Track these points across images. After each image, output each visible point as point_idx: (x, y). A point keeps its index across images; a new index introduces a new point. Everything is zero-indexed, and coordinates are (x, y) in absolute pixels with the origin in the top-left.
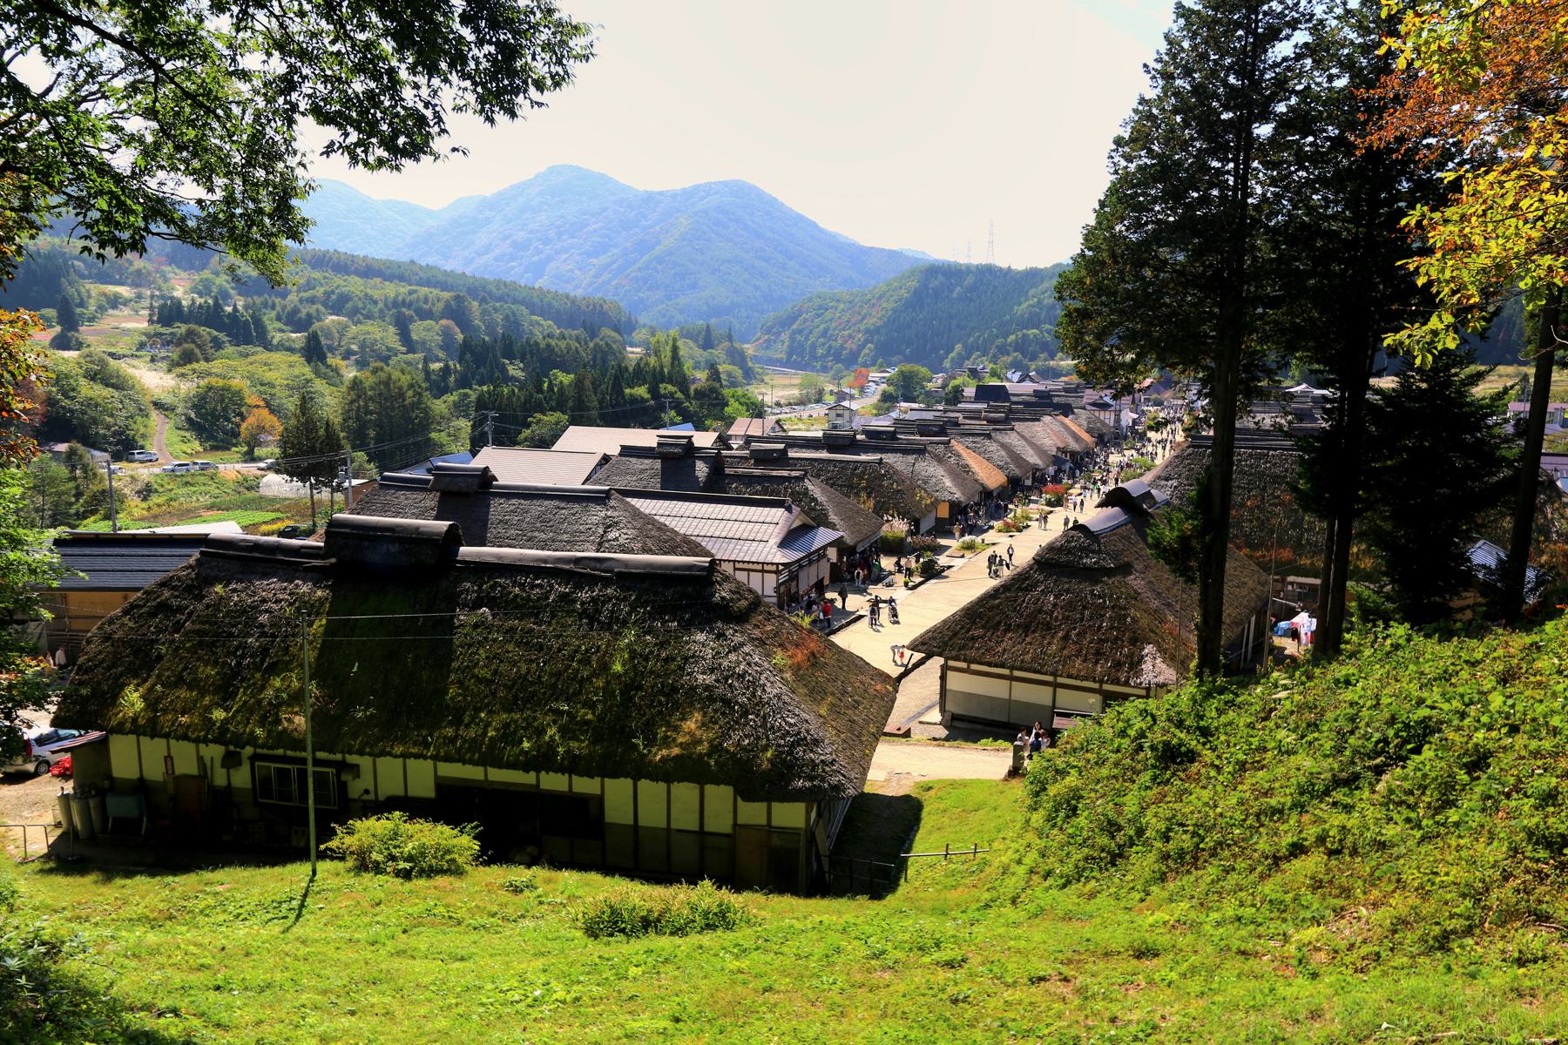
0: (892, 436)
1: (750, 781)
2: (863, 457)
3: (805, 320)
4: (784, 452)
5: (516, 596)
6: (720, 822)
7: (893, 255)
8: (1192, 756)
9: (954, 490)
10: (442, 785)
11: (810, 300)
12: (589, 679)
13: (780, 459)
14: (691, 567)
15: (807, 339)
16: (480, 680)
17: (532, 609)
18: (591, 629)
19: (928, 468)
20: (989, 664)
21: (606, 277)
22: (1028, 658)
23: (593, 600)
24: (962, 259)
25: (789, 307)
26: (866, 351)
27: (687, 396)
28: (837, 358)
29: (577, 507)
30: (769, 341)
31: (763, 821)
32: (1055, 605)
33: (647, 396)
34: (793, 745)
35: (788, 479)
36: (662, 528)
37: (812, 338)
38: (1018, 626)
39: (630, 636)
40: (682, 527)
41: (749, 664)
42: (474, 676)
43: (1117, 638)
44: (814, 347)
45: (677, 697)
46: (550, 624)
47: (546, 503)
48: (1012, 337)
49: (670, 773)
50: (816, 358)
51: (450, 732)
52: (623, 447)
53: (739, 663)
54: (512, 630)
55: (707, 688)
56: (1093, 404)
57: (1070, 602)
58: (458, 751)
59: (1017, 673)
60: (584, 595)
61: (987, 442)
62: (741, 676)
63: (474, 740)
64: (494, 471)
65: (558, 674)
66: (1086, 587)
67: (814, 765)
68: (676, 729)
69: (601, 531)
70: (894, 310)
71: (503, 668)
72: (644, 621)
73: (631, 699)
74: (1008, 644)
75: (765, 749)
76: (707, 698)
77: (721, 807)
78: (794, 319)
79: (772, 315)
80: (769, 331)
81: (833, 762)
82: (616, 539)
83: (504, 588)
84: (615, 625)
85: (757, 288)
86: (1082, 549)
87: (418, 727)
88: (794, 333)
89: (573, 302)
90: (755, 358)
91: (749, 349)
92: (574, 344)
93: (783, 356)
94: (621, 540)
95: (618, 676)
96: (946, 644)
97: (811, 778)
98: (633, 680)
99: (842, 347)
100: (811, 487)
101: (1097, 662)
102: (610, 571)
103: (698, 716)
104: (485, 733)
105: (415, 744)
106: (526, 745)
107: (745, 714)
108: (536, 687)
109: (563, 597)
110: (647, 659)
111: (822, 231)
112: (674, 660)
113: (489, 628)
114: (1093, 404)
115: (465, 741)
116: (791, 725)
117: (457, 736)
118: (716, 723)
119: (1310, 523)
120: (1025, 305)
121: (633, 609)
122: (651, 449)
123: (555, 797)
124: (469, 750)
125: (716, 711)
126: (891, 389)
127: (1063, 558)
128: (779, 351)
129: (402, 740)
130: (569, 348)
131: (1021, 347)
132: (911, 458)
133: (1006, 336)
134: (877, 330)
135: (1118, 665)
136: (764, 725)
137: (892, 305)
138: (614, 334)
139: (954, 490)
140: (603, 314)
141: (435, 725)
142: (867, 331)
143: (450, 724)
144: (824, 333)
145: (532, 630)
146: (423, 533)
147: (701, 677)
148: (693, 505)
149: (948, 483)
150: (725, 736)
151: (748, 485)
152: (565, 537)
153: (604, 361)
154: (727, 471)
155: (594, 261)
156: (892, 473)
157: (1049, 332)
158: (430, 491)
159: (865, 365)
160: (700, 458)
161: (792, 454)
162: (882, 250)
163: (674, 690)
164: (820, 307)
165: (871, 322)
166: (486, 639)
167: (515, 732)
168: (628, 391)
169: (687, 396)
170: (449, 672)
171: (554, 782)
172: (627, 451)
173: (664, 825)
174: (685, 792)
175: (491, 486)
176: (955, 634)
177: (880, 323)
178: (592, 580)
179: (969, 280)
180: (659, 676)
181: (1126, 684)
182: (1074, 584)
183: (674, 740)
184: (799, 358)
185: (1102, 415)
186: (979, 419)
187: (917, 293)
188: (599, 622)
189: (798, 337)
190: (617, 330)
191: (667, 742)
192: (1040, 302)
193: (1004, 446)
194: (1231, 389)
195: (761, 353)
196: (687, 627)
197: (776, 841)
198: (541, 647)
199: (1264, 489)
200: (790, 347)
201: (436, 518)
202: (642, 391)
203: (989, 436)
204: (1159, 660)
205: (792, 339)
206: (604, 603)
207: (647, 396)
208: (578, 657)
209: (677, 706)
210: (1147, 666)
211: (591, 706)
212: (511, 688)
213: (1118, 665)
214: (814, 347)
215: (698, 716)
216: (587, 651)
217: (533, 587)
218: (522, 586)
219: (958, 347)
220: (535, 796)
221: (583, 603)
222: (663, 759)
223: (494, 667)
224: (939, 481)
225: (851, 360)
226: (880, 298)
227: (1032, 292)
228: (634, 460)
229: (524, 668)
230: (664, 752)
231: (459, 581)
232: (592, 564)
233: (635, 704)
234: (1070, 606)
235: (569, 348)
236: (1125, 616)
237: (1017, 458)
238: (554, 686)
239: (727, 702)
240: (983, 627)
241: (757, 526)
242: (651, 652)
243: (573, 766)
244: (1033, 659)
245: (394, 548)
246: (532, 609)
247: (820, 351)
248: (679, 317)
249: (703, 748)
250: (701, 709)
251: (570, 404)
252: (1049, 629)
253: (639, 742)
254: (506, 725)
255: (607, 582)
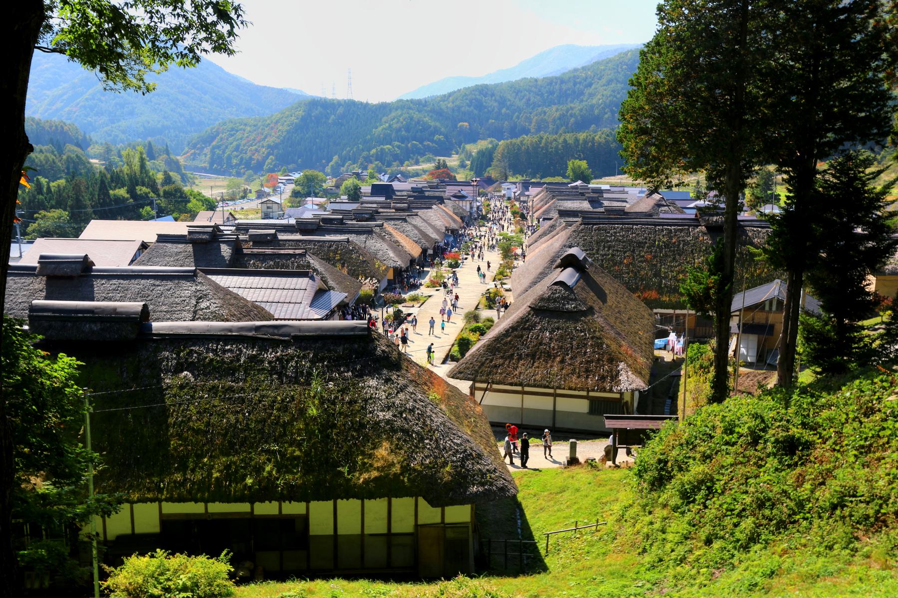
0: (341, 221)
1: (440, 494)
2: (328, 238)
3: (222, 139)
4: (275, 236)
5: (212, 360)
6: (403, 523)
7: (281, 92)
8: (808, 445)
9: (396, 259)
10: (166, 521)
11: (225, 124)
12: (290, 423)
13: (272, 241)
14: (354, 328)
15: (224, 152)
16: (197, 432)
17: (229, 370)
18: (282, 383)
19: (374, 244)
20: (511, 384)
21: (59, 105)
22: (538, 377)
23: (278, 359)
24: (329, 96)
25: (209, 129)
26: (269, 161)
27: (158, 195)
28: (248, 166)
29: (170, 284)
30: (194, 154)
31: (438, 520)
32: (551, 339)
33: (127, 196)
34: (463, 460)
35: (294, 255)
36: (236, 297)
37: (228, 152)
38: (527, 355)
39: (316, 386)
40: (250, 296)
41: (415, 401)
42: (190, 428)
43: (599, 360)
44: (229, 158)
45: (366, 433)
46: (245, 381)
47: (143, 281)
48: (374, 151)
49: (365, 493)
50: (232, 167)
51: (178, 477)
52: (159, 236)
53: (407, 401)
54: (214, 389)
55: (388, 422)
56: (455, 196)
57: (562, 336)
58: (189, 492)
59: (527, 389)
60: (270, 355)
61: (404, 224)
62: (412, 411)
63: (202, 482)
64: (92, 258)
65: (264, 421)
66: (571, 325)
67: (483, 475)
68: (370, 456)
69: (194, 302)
70: (288, 132)
71: (214, 420)
72: (324, 373)
73: (328, 436)
74: (524, 370)
75: (445, 464)
76: (391, 430)
77: (406, 514)
78: (214, 138)
79: (195, 135)
80: (194, 146)
81: (495, 471)
82: (208, 308)
83: (199, 354)
84: (303, 379)
85: (181, 115)
86: (564, 298)
87: (150, 476)
88: (214, 148)
89: (38, 124)
90: (186, 167)
91: (181, 159)
92: (51, 157)
93: (207, 165)
94: (212, 309)
95: (314, 419)
96: (477, 371)
97: (483, 484)
98: (328, 421)
99: (251, 159)
100: (312, 261)
101: (587, 377)
102: (288, 335)
103: (386, 444)
104: (210, 475)
105: (149, 490)
106: (249, 481)
107: (422, 439)
108: (246, 433)
109: (252, 358)
110: (334, 403)
111: (228, 74)
112: (356, 402)
113: (194, 388)
114: (455, 196)
115: (193, 483)
116: (458, 445)
117: (185, 480)
118: (401, 449)
119: (665, 273)
120: (380, 128)
121: (313, 362)
122: (184, 236)
123: (267, 520)
124: (199, 490)
125: (399, 439)
126: (299, 188)
127: (552, 306)
128: (203, 161)
129: (138, 488)
130: (47, 160)
131: (380, 157)
132: (363, 238)
133: (369, 151)
134: (276, 146)
135: (603, 378)
136: (437, 447)
137: (285, 128)
138: (76, 149)
139: (396, 259)
140: (63, 133)
141: (165, 470)
142: (269, 146)
143: (177, 470)
144: (237, 148)
145: (231, 388)
146: (121, 313)
147: (381, 414)
148: (295, 279)
149: (391, 254)
150: (410, 458)
151: (263, 261)
152: (164, 308)
153: (75, 168)
154: (245, 251)
155: (48, 92)
156: (357, 250)
157: (399, 147)
158: (37, 276)
159: (271, 170)
160: (224, 242)
161: (282, 237)
162: (273, 89)
163: (362, 426)
164: (232, 129)
165: (271, 140)
166: (193, 397)
167: (236, 471)
168: (111, 192)
169: (158, 195)
170: (168, 427)
171: (266, 508)
172: (163, 239)
173: (331, 532)
174: (376, 507)
175: (91, 270)
176: (483, 364)
177: (278, 141)
178: (274, 344)
179: (340, 110)
180: (347, 416)
181: (611, 391)
182: (561, 323)
183: (371, 465)
184: (218, 167)
185: (461, 203)
186: (390, 208)
187: (303, 119)
188: (287, 377)
189: (217, 151)
190: (78, 145)
191: (365, 468)
192: (390, 126)
193: (415, 226)
194: (729, 182)
195: (189, 163)
196: (360, 375)
197: (450, 534)
198: (242, 400)
199: (633, 251)
200: (212, 158)
201: (46, 298)
202: (122, 192)
203: (405, 220)
204: (630, 373)
205: (213, 153)
206: (288, 361)
207: (127, 196)
208: (277, 406)
209: (367, 438)
210: (623, 377)
211: (299, 445)
212: (225, 435)
213: (603, 378)
214: (229, 158)
215: (386, 444)
216: (283, 400)
217: (224, 352)
218: (215, 351)
219: (336, 158)
220: (251, 520)
221: (270, 363)
222: (366, 482)
223: (205, 420)
224: (385, 254)
225: (258, 168)
226: (277, 122)
227: (384, 119)
228: (169, 245)
229: (232, 419)
230: (366, 476)
231: (158, 350)
232: (271, 330)
233: (333, 439)
234: (561, 338)
235: (47, 160)
236: (602, 344)
237: (425, 235)
238: (261, 431)
239: (406, 432)
240: (502, 357)
241: (280, 291)
242: (336, 397)
243: (292, 494)
244: (542, 378)
245: (96, 327)
246: (229, 370)
247: (234, 161)
248: (122, 136)
249: (397, 469)
250: (387, 439)
251: (70, 203)
252: (549, 356)
253: (345, 470)
254: (227, 467)
255: (286, 345)
